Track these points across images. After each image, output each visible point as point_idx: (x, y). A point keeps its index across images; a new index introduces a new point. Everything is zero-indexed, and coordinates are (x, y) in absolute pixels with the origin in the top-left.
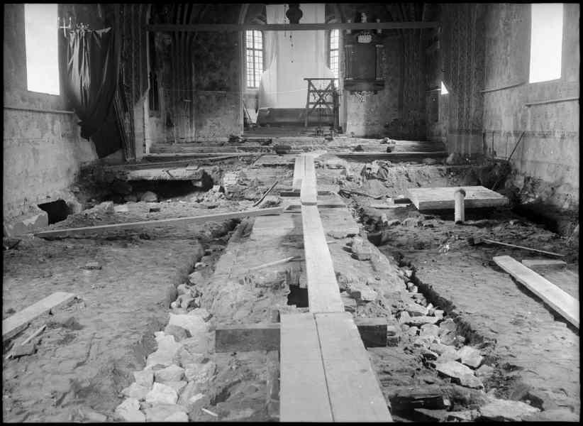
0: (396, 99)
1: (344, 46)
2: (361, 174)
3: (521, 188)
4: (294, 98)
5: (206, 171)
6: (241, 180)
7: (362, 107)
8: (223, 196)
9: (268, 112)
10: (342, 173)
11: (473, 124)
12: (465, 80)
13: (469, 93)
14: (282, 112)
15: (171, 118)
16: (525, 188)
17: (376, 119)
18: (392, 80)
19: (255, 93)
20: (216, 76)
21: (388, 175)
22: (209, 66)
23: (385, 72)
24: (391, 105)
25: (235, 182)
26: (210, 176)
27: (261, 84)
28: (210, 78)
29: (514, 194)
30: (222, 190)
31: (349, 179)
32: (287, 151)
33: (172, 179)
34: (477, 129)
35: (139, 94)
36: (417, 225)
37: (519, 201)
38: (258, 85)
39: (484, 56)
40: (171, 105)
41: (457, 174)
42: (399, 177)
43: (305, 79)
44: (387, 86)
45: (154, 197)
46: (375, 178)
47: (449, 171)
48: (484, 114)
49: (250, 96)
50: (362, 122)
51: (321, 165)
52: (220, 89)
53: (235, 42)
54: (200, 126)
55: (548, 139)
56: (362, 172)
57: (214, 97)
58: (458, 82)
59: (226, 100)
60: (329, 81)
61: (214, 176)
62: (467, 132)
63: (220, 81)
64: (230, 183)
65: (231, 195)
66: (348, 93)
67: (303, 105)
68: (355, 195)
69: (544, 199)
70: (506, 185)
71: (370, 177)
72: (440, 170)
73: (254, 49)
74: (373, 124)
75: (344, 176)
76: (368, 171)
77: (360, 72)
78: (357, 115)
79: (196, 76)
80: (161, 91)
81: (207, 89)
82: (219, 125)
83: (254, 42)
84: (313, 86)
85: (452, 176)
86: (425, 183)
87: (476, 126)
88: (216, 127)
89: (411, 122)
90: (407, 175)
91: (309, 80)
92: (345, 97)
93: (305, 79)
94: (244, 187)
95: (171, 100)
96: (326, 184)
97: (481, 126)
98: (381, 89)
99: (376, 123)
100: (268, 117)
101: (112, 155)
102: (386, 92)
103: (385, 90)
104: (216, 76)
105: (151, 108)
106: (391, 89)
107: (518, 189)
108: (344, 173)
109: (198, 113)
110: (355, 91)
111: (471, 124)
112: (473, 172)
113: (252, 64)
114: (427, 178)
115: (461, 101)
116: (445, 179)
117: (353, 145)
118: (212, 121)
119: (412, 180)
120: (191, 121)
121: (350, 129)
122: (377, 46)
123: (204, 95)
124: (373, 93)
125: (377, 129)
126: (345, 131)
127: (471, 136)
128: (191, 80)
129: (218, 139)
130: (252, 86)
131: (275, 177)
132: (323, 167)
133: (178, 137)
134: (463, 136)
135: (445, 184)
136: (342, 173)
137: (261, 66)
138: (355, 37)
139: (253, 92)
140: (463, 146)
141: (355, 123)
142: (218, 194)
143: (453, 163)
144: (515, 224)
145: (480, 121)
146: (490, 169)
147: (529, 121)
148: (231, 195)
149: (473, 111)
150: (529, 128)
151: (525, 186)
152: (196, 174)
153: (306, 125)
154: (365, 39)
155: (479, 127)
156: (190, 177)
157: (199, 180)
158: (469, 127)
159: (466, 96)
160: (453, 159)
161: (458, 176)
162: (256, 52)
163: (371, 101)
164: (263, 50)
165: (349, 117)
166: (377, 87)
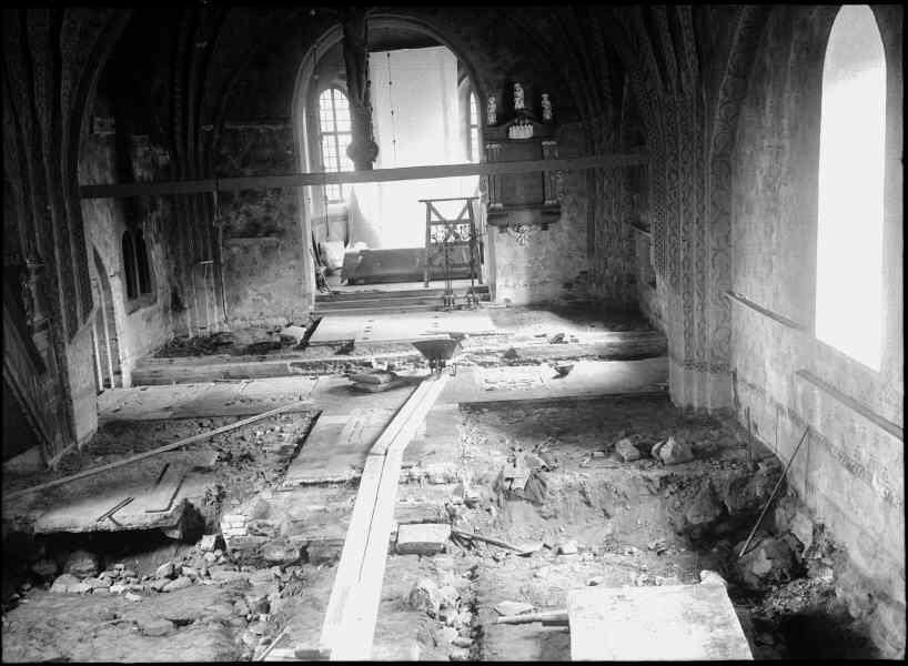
2: (495, 490)
6: (255, 526)
7: (521, 250)
8: (222, 559)
9: (360, 258)
10: (456, 492)
12: (695, 271)
13: (702, 296)
15: (180, 295)
18: (575, 203)
20: (258, 210)
24: (574, 246)
25: (242, 532)
26: (198, 510)
28: (248, 214)
30: (220, 544)
31: (470, 504)
32: (372, 388)
33: (120, 528)
40: (177, 271)
44: (565, 215)
45: (88, 564)
46: (521, 499)
52: (267, 235)
53: (288, 148)
57: (257, 247)
58: (682, 275)
59: (279, 252)
60: (465, 202)
61: (206, 511)
62: (702, 367)
64: (232, 532)
65: (237, 555)
66: (496, 230)
67: (419, 242)
68: (481, 543)
71: (510, 495)
73: (335, 133)
74: (543, 283)
75: (460, 499)
78: (513, 267)
80: (156, 254)
81: (243, 235)
82: (269, 297)
84: (437, 214)
87: (719, 358)
88: (265, 300)
90: (583, 493)
91: (429, 203)
92: (491, 240)
94: (262, 539)
95: (177, 264)
98: (554, 221)
99: (548, 280)
100: (360, 267)
101: (20, 456)
103: (562, 221)
104: (258, 210)
105: (130, 294)
106: (571, 219)
108: (459, 491)
109: (226, 277)
110: (507, 226)
112: (712, 487)
113: (334, 149)
114: (623, 499)
115: (688, 307)
118: (255, 290)
119: (593, 504)
122: (544, 143)
124: (539, 228)
125: (552, 291)
126: (494, 297)
129: (269, 321)
131: (325, 510)
132: (419, 481)
133: (194, 327)
134: (695, 373)
136: (456, 492)
138: (502, 128)
140: (695, 390)
141: (511, 284)
142: (210, 557)
143: (673, 460)
145: (726, 350)
148: (237, 555)
154: (521, 132)
157: (175, 527)
158: (706, 359)
160: (673, 453)
165: (499, 272)
166: (547, 215)
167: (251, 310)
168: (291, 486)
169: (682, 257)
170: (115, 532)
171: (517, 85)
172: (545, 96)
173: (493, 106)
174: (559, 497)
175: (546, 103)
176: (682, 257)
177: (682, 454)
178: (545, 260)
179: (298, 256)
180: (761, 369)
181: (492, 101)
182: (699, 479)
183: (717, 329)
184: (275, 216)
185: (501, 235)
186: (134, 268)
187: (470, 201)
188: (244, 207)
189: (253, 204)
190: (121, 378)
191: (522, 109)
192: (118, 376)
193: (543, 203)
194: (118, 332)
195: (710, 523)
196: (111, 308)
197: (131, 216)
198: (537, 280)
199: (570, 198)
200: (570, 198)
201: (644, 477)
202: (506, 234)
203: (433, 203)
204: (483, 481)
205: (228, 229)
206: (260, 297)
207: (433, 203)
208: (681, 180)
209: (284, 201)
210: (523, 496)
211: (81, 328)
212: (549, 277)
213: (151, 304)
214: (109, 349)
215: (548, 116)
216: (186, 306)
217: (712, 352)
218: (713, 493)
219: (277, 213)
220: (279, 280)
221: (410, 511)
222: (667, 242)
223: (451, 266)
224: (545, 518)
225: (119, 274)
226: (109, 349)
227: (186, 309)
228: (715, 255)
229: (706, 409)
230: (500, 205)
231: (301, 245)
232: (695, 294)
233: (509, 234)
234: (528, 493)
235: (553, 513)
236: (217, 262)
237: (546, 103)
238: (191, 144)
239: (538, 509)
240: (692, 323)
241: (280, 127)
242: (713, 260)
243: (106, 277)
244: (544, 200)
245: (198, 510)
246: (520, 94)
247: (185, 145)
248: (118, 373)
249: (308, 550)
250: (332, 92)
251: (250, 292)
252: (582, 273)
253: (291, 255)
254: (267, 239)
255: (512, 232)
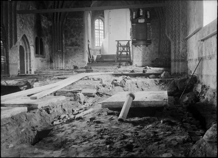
0: (158, 49)
1: (132, 24)
2: (112, 84)
3: (200, 92)
4: (111, 50)
5: (28, 81)
9: (101, 56)
11: (182, 57)
14: (107, 56)
15: (52, 59)
16: (202, 92)
17: (147, 58)
19: (99, 49)
21: (126, 84)
22: (70, 36)
23: (151, 36)
27: (102, 45)
28: (71, 41)
29: (195, 96)
31: (104, 86)
34: (184, 59)
35: (12, 44)
36: (89, 121)
37: (198, 100)
38: (101, 46)
39: (187, 19)
40: (52, 52)
41: (165, 83)
42: (132, 85)
43: (116, 41)
44: (153, 43)
47: (161, 81)
48: (188, 50)
49: (97, 50)
50: (141, 59)
51: (89, 78)
52: (76, 46)
54: (67, 62)
55: (212, 60)
56: (113, 82)
60: (128, 42)
62: (179, 61)
63: (76, 42)
66: (134, 46)
68: (104, 95)
69: (209, 100)
70: (194, 90)
71: (116, 85)
72: (156, 81)
73: (99, 30)
74: (146, 61)
75: (101, 84)
76: (115, 82)
77: (140, 35)
79: (65, 40)
80: (46, 47)
81: (70, 46)
82: (75, 62)
83: (99, 27)
85: (162, 85)
86: (146, 89)
87: (183, 57)
89: (164, 59)
90: (136, 84)
91: (118, 41)
92: (133, 48)
93: (116, 41)
95: (52, 50)
96: (90, 88)
97: (186, 57)
98: (149, 44)
100: (101, 58)
102: (152, 46)
104: (74, 40)
105: (37, 52)
106: (154, 44)
107: (198, 93)
108: (101, 83)
110: (137, 45)
111: (180, 56)
113: (99, 36)
114: (147, 85)
116: (158, 87)
117: (130, 70)
118: (72, 60)
119: (139, 87)
120: (62, 60)
121: (134, 63)
122: (147, 24)
123: (68, 48)
124: (146, 46)
127: (181, 63)
128: (62, 42)
130: (99, 46)
132: (90, 80)
134: (177, 63)
135: (158, 89)
137: (103, 37)
138: (136, 20)
139: (99, 48)
143: (164, 77)
144: (164, 122)
146: (184, 80)
147: (204, 53)
149: (181, 49)
150: (204, 55)
151: (202, 91)
152: (19, 82)
153: (116, 62)
154: (141, 21)
155: (185, 58)
156: (17, 84)
159: (177, 41)
160: (164, 75)
161: (166, 84)
162: (100, 31)
163: (145, 50)
164: (104, 30)
165: (134, 57)
166: (148, 43)
167: (70, 65)
168: (55, 78)
169: (174, 30)
170: (6, 86)
171: (141, 9)
172: (148, 12)
173: (134, 15)
174: (130, 85)
175: (148, 14)
176: (174, 30)
177: (167, 76)
178: (146, 55)
179: (83, 52)
180: (192, 54)
181: (134, 13)
182: (171, 81)
183: (183, 49)
184: (78, 41)
185: (135, 47)
186: (39, 47)
187: (129, 41)
188: (70, 39)
189: (73, 38)
190: (31, 72)
191: (142, 15)
192: (30, 71)
193: (147, 39)
194: (31, 60)
195: (173, 92)
196: (30, 54)
197: (39, 30)
198: (144, 60)
199: (154, 39)
200: (154, 39)
201: (155, 80)
202: (136, 47)
203: (119, 42)
204: (109, 81)
205: (66, 44)
206: (73, 62)
207: (119, 42)
208: (173, 8)
209: (81, 37)
210: (119, 85)
211: (14, 46)
212: (148, 59)
213: (43, 58)
214: (28, 64)
215: (149, 17)
216: (53, 61)
217: (181, 55)
218: (174, 84)
219: (79, 40)
220: (78, 58)
221: (86, 86)
222: (170, 26)
223: (122, 59)
224: (125, 91)
225: (33, 46)
226: (28, 64)
227: (53, 62)
228: (182, 28)
229: (180, 73)
230: (135, 40)
231: (84, 49)
232: (177, 40)
233: (137, 47)
234: (121, 84)
235: (127, 89)
236: (62, 51)
237: (148, 14)
238: (58, 22)
239: (123, 88)
240: (176, 48)
241: (81, 19)
242: (182, 29)
243: (29, 45)
244: (147, 39)
245: (30, 84)
246: (141, 11)
247: (57, 22)
248: (30, 70)
249: (56, 94)
250: (99, 20)
251: (70, 60)
252: (156, 58)
253: (81, 51)
254: (75, 47)
255: (138, 47)
